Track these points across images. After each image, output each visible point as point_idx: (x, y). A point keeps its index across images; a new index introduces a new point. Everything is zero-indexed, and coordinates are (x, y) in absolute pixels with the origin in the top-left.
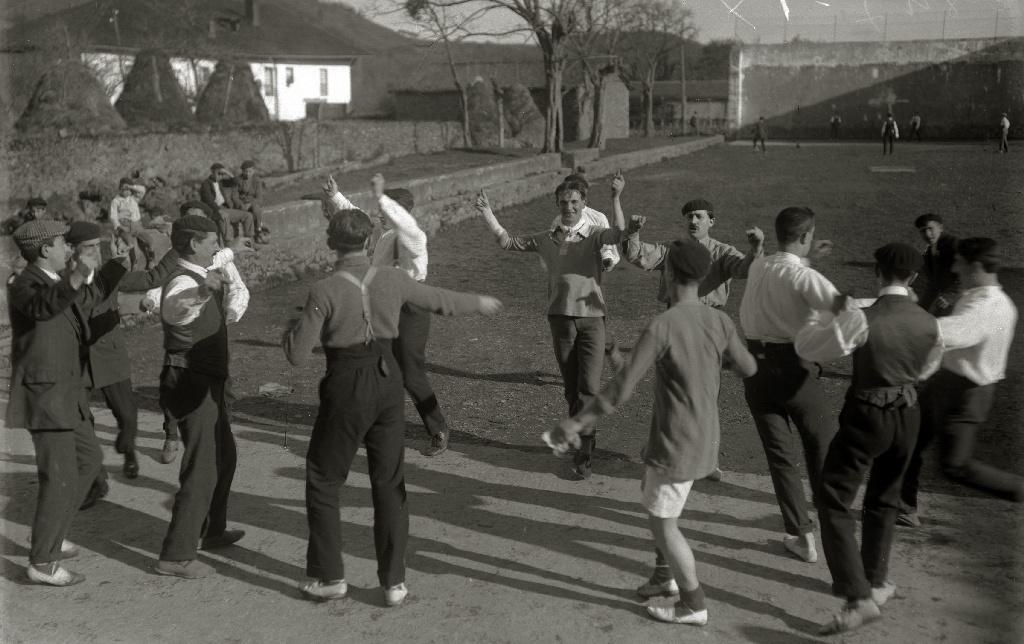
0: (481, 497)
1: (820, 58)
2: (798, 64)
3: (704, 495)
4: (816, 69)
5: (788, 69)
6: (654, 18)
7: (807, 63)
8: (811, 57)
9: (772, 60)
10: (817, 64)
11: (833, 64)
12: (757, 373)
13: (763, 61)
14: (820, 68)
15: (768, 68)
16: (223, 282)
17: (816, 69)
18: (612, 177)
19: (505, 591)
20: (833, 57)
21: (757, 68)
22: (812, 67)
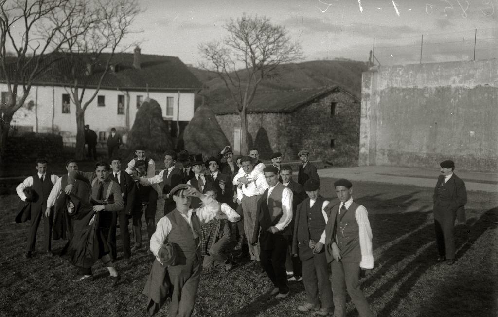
0: (49, 206)
1: (457, 80)
2: (433, 85)
3: (64, 246)
4: (453, 91)
5: (423, 91)
6: (64, 6)
7: (444, 84)
8: (448, 78)
9: (407, 82)
10: (453, 86)
11: (471, 85)
12: (361, 204)
13: (398, 83)
14: (457, 89)
15: (403, 90)
16: (279, 137)
17: (453, 91)
18: (85, 129)
19: (492, 186)
20: (472, 76)
21: (392, 89)
22: (448, 88)
